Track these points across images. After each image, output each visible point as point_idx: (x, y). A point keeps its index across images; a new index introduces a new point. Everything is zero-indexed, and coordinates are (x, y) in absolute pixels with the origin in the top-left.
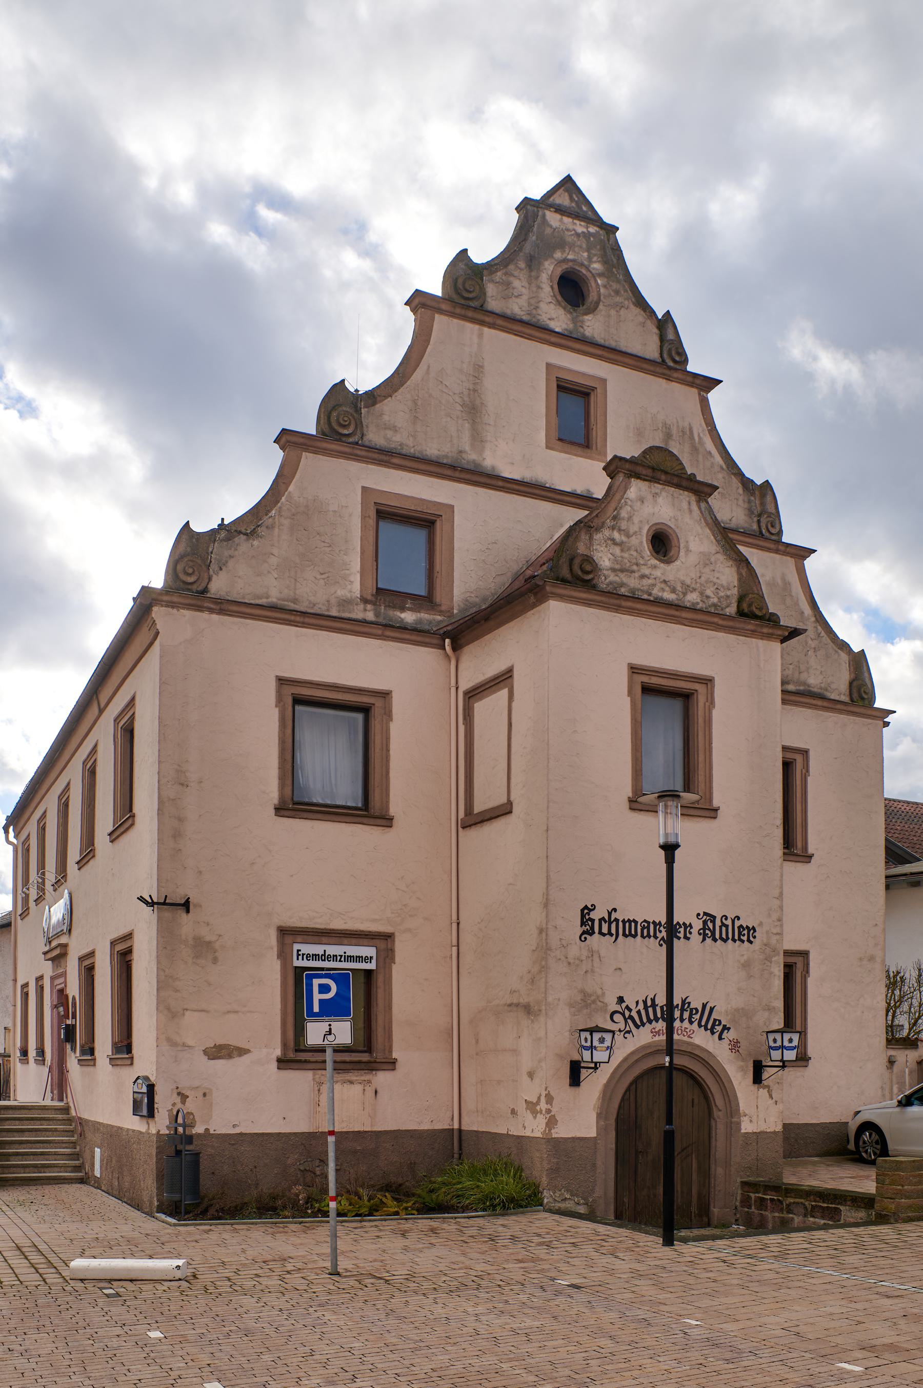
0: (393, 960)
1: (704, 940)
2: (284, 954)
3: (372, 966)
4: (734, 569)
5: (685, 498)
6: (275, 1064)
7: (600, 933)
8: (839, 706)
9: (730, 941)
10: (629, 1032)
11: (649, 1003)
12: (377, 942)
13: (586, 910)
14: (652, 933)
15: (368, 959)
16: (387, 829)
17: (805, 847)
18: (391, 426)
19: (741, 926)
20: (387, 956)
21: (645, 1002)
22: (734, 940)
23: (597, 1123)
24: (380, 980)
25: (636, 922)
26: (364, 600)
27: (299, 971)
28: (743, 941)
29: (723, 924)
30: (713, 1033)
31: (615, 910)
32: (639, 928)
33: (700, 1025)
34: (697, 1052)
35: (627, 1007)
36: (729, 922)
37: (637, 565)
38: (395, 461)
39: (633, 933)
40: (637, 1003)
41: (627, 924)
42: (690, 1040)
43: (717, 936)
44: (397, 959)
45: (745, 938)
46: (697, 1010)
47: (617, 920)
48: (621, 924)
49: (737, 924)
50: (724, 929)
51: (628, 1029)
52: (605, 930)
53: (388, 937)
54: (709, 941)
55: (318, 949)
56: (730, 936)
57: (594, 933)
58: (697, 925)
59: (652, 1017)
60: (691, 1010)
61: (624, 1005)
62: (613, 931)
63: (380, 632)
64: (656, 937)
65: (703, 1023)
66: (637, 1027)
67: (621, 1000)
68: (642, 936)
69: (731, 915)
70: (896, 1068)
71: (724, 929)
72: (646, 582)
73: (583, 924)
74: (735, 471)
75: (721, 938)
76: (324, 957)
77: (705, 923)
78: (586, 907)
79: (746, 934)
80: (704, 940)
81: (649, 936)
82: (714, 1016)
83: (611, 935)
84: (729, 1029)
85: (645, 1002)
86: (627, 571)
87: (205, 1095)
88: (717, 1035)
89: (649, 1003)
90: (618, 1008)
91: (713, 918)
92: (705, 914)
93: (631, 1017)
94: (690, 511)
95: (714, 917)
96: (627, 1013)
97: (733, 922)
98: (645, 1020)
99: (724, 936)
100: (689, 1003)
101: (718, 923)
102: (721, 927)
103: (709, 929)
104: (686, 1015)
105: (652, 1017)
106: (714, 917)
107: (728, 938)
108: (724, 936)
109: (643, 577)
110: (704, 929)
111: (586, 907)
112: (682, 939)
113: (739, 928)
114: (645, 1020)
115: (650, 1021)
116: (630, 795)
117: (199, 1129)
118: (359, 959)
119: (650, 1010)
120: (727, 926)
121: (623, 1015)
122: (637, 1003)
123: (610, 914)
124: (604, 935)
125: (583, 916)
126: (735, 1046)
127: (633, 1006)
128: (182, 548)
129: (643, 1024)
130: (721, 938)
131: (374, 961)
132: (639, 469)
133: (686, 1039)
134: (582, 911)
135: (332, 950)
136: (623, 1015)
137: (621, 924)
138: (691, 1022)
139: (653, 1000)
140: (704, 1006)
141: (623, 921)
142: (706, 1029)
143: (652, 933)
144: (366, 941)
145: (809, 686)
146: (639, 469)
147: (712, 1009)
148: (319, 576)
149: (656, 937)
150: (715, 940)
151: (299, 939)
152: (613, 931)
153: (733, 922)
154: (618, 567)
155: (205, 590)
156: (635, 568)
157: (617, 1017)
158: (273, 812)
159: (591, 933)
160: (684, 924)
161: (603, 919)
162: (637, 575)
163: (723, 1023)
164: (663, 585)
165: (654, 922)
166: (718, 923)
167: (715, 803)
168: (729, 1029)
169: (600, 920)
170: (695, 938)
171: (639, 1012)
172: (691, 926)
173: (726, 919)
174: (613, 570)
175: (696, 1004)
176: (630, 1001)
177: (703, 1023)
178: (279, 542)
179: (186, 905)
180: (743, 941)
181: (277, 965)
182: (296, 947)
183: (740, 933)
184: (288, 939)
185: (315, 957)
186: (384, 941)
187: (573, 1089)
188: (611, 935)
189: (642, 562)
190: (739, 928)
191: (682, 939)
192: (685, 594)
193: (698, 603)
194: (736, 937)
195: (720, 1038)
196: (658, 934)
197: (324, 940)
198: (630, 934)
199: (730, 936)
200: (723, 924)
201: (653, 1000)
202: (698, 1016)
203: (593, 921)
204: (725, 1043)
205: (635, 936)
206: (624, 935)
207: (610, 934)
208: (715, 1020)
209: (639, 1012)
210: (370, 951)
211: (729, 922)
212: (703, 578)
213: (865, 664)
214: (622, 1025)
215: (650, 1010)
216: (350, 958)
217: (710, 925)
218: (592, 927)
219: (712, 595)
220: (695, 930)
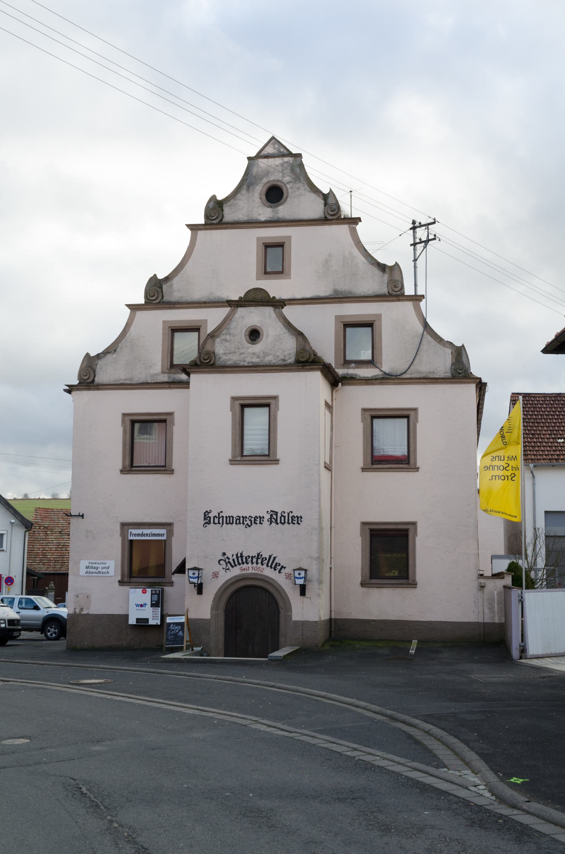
0: (173, 535)
1: (271, 524)
2: (123, 534)
3: (164, 538)
4: (294, 339)
5: (269, 311)
6: (118, 583)
7: (214, 523)
8: (439, 381)
9: (286, 524)
10: (228, 569)
11: (239, 555)
12: (166, 527)
13: (206, 514)
14: (241, 522)
15: (162, 535)
16: (171, 475)
17: (415, 463)
18: (175, 292)
19: (293, 516)
20: (170, 533)
21: (237, 555)
22: (289, 523)
23: (211, 612)
24: (167, 543)
25: (233, 517)
26: (163, 372)
27: (131, 541)
28: (294, 524)
29: (282, 516)
30: (275, 570)
31: (222, 512)
32: (235, 520)
33: (267, 566)
34: (266, 579)
35: (227, 558)
36: (286, 515)
37: (238, 349)
38: (176, 306)
39: (231, 522)
40: (233, 555)
41: (228, 519)
42: (261, 573)
43: (279, 521)
44: (175, 534)
45: (296, 522)
46: (266, 559)
47: (223, 517)
48: (225, 518)
49: (291, 515)
50: (283, 518)
51: (227, 568)
52: (216, 521)
53: (170, 524)
54: (273, 524)
55: (139, 531)
56: (286, 521)
57: (210, 523)
58: (267, 517)
59: (240, 562)
60: (263, 558)
61: (226, 557)
62: (221, 522)
63: (168, 386)
64: (243, 523)
65: (270, 565)
66: (233, 567)
67: (224, 554)
68: (236, 523)
69: (287, 511)
70: (486, 590)
71: (283, 518)
72: (242, 356)
73: (205, 519)
74: (373, 262)
75: (281, 522)
76: (142, 535)
77: (271, 515)
78: (207, 512)
79: (296, 520)
80: (271, 524)
81: (240, 523)
82: (276, 561)
83: (220, 524)
84: (285, 568)
85: (237, 555)
86: (232, 353)
87: (88, 597)
88: (277, 571)
89: (239, 555)
90: (223, 558)
91: (276, 513)
92: (271, 511)
93: (229, 562)
94: (270, 316)
95: (277, 513)
96: (227, 561)
97: (288, 514)
98: (237, 563)
99: (283, 521)
100: (262, 555)
101: (279, 515)
102: (281, 518)
103: (274, 518)
104: (260, 561)
105: (240, 562)
106: (277, 513)
107: (285, 522)
108: (283, 521)
109: (241, 354)
110: (271, 518)
111: (207, 512)
112: (258, 524)
113: (292, 517)
114: (237, 563)
115: (239, 564)
116: (230, 458)
117: (85, 612)
118: (158, 535)
119: (240, 559)
120: (285, 517)
121: (225, 561)
122: (233, 555)
123: (219, 514)
124: (216, 524)
125: (205, 515)
126: (288, 576)
127: (230, 557)
128: (85, 365)
129: (236, 566)
130: (281, 522)
131: (165, 536)
132: (241, 303)
133: (259, 572)
134: (205, 513)
135: (146, 531)
136: (225, 561)
137: (225, 518)
138: (262, 564)
139: (241, 554)
140: (270, 557)
141: (226, 517)
142: (271, 568)
143: (241, 522)
144: (161, 527)
145: (421, 373)
146: (241, 303)
147: (275, 558)
148: (142, 366)
149: (243, 523)
150: (277, 524)
151: (131, 527)
152: (221, 522)
153: (288, 514)
154: (228, 352)
155: (93, 381)
156: (237, 350)
157: (222, 562)
158: (119, 472)
159: (209, 523)
160: (260, 517)
161: (216, 516)
162: (237, 354)
163: (281, 565)
164: (252, 356)
165: (243, 517)
166: (279, 515)
167: (278, 457)
168: (285, 568)
169: (214, 517)
170: (266, 523)
171: (233, 560)
172: (263, 517)
173: (284, 513)
174: (225, 354)
175: (266, 555)
176: (229, 554)
177: (270, 565)
178: (123, 356)
179: (82, 516)
180: (294, 524)
181: (119, 539)
182: (130, 531)
183: (292, 520)
184: (126, 528)
185: (138, 535)
186: (168, 526)
187: (199, 596)
188: (220, 524)
189: (241, 347)
190: (292, 517)
191: (258, 524)
192: (264, 358)
193: (272, 361)
194: (290, 521)
195: (280, 572)
196: (245, 522)
197: (142, 527)
198: (230, 523)
199: (286, 521)
200: (282, 516)
201: (241, 554)
202: (266, 561)
203: (210, 518)
204: (283, 575)
205: (232, 524)
206: (227, 523)
207: (219, 523)
208: (276, 564)
209: (233, 560)
210: (163, 531)
211: (286, 515)
212: (276, 348)
213: (464, 352)
214: (224, 566)
215: (240, 559)
216: (154, 535)
217: (275, 517)
218: (210, 521)
219: (280, 355)
220: (265, 520)
